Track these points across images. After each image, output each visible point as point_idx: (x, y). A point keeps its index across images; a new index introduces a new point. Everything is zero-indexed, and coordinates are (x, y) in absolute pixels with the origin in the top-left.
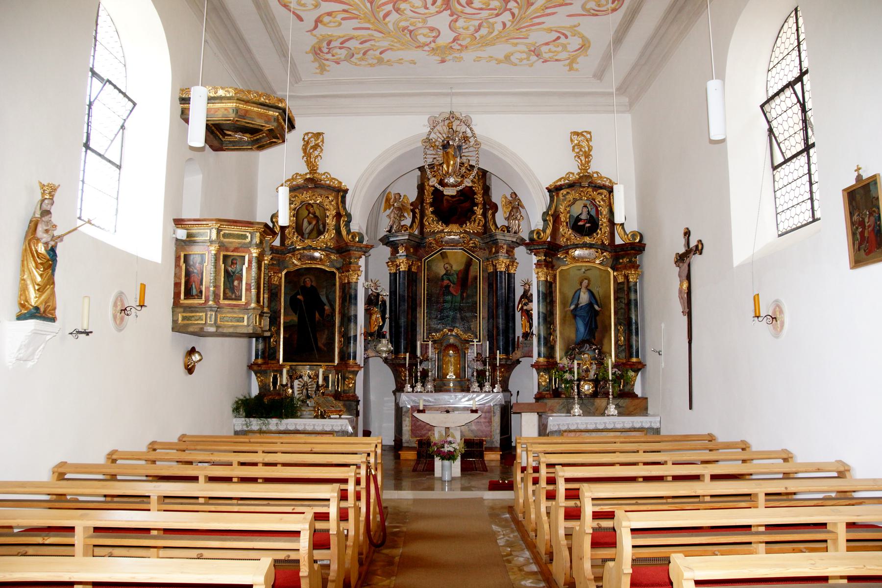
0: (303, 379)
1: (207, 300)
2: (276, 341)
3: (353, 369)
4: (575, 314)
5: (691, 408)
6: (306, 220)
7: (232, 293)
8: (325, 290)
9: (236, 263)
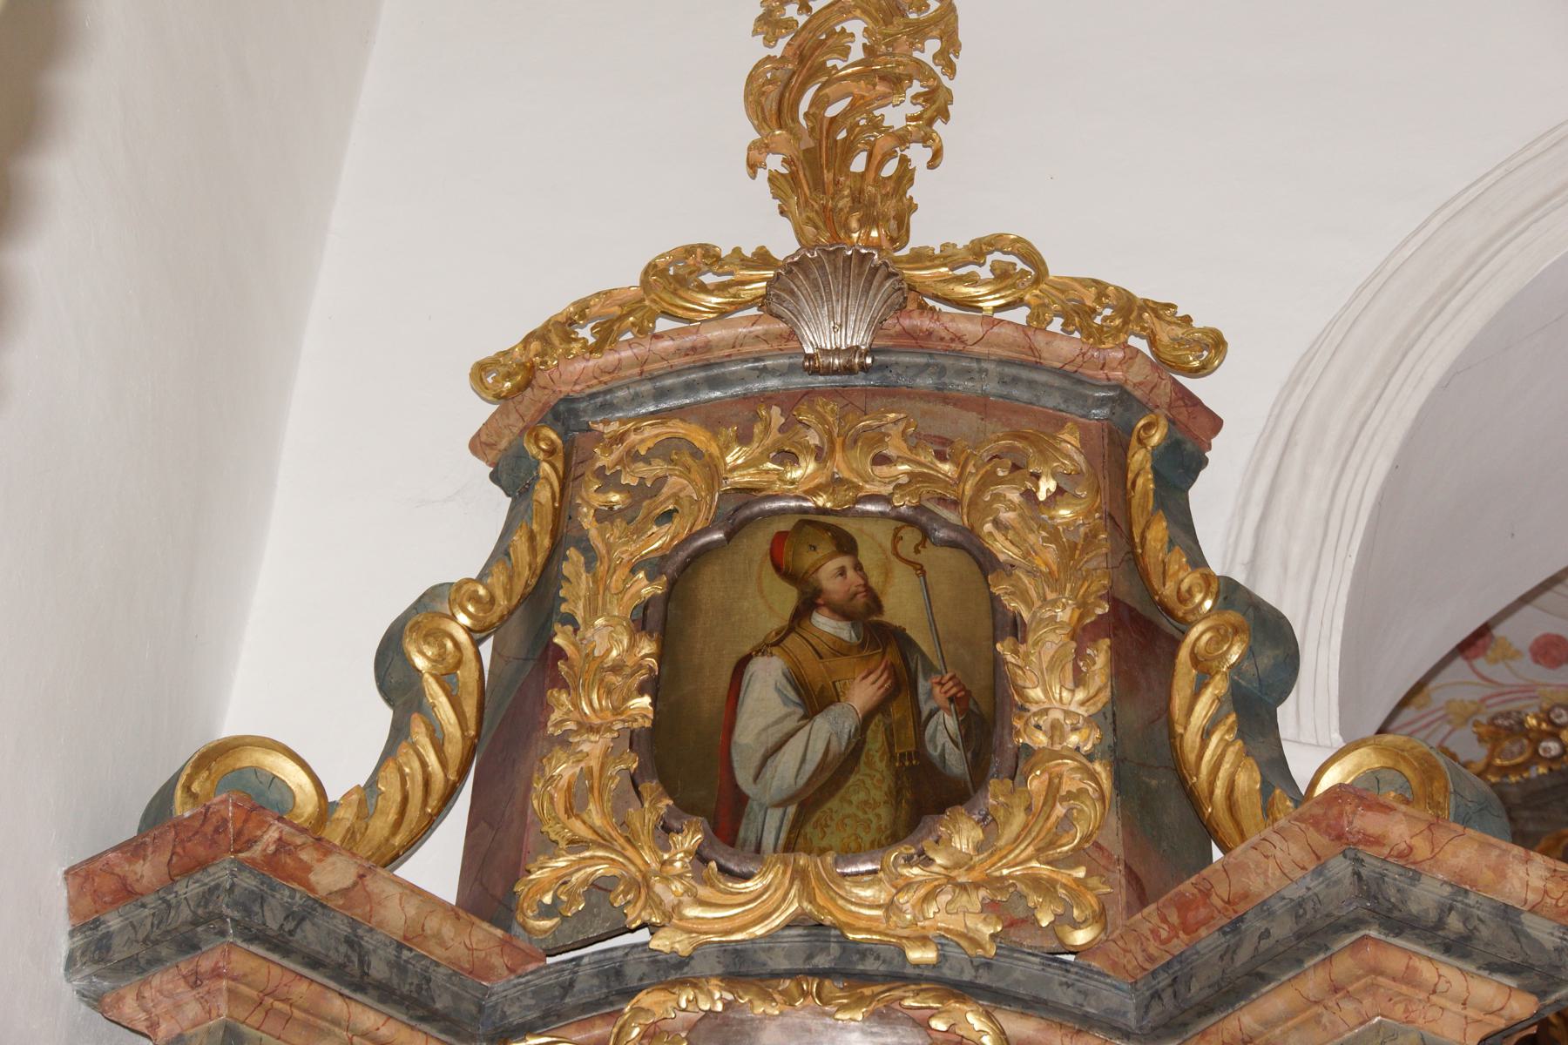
6: (767, 676)
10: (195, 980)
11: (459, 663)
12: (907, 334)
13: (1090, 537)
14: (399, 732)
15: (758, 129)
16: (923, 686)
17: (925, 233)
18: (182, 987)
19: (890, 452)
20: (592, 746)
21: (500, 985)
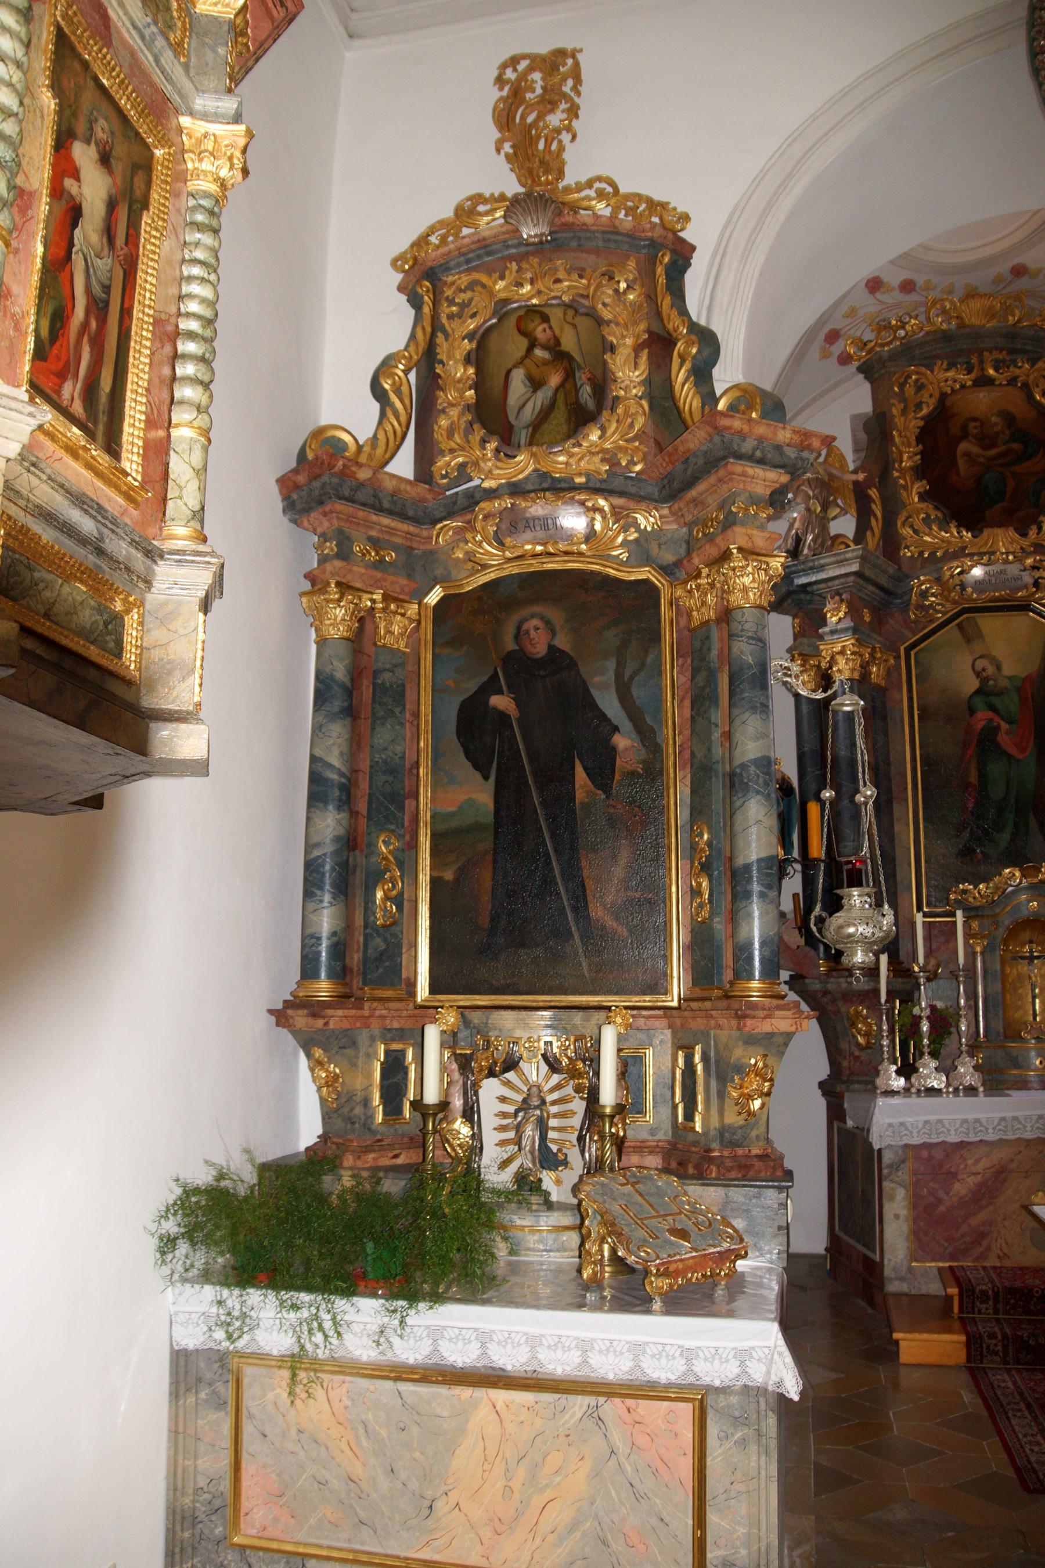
0: (522, 1075)
2: (398, 901)
3: (766, 1027)
6: (518, 377)
8: (611, 664)
10: (325, 514)
11: (401, 384)
12: (565, 225)
13: (640, 306)
14: (383, 414)
15: (500, 131)
16: (577, 375)
17: (570, 178)
18: (321, 517)
19: (561, 277)
20: (454, 412)
21: (431, 504)
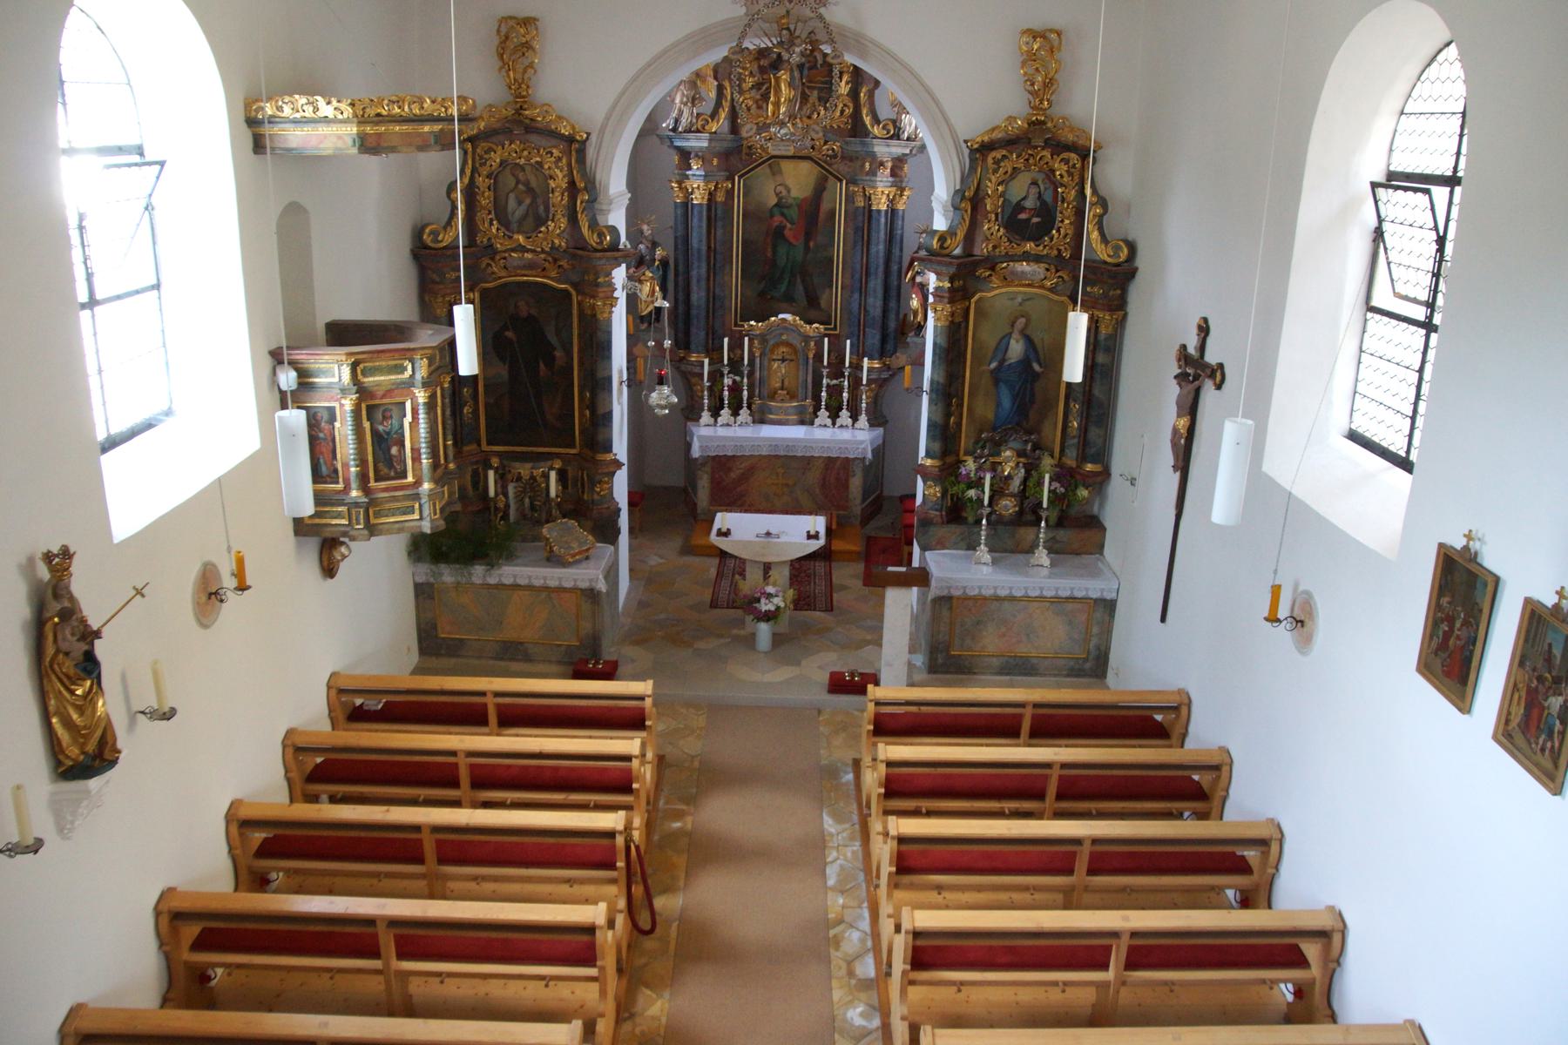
1: (347, 489)
4: (996, 377)
5: (1163, 619)
6: (512, 196)
7: (390, 469)
9: (391, 417)
